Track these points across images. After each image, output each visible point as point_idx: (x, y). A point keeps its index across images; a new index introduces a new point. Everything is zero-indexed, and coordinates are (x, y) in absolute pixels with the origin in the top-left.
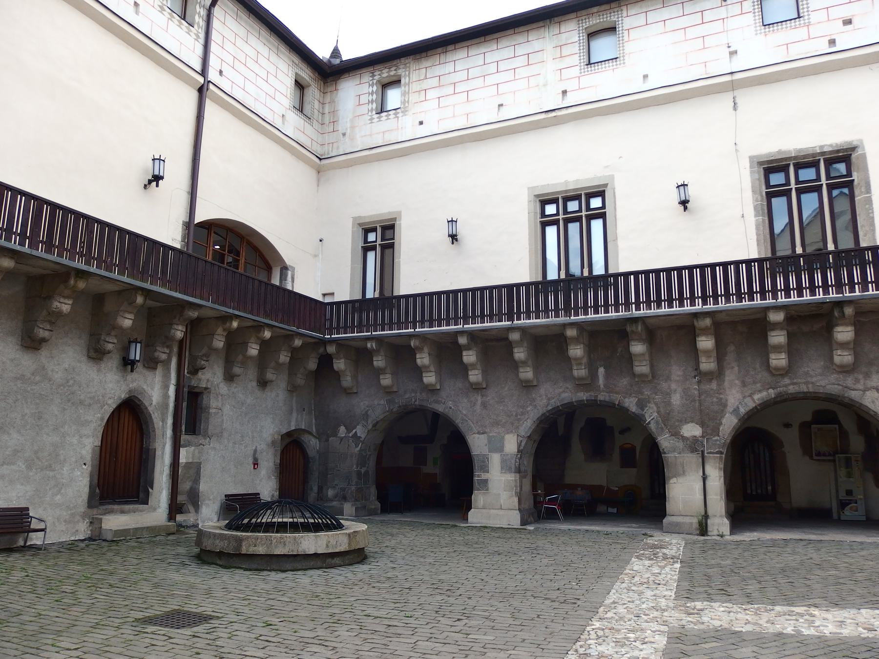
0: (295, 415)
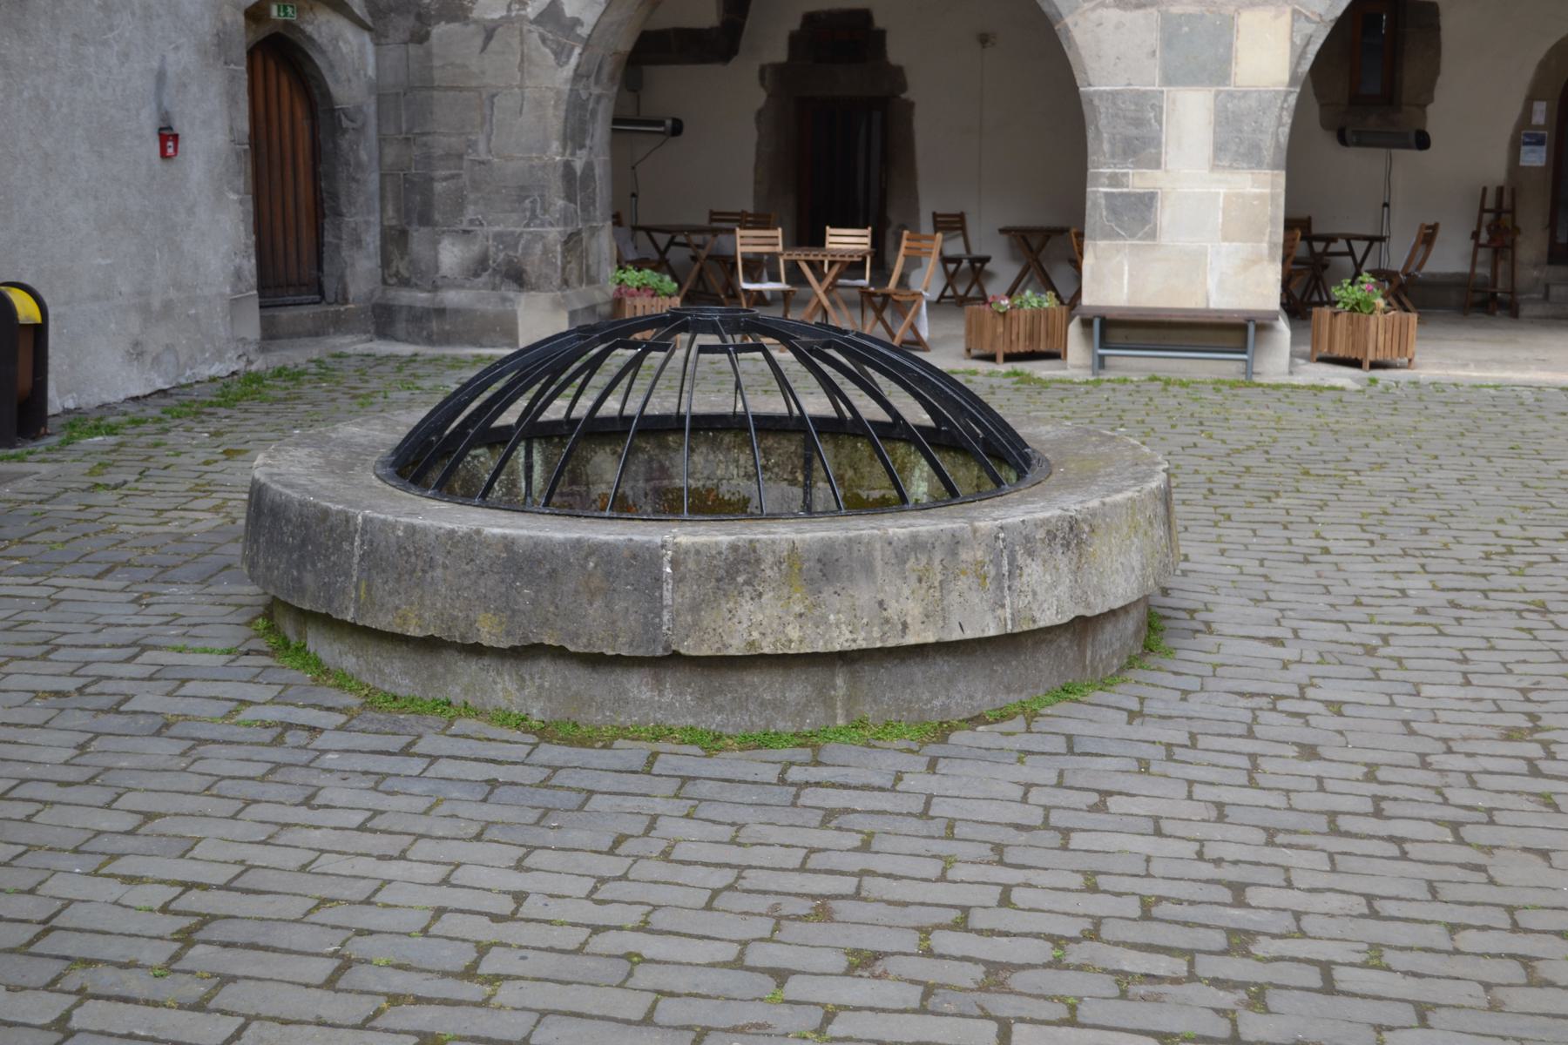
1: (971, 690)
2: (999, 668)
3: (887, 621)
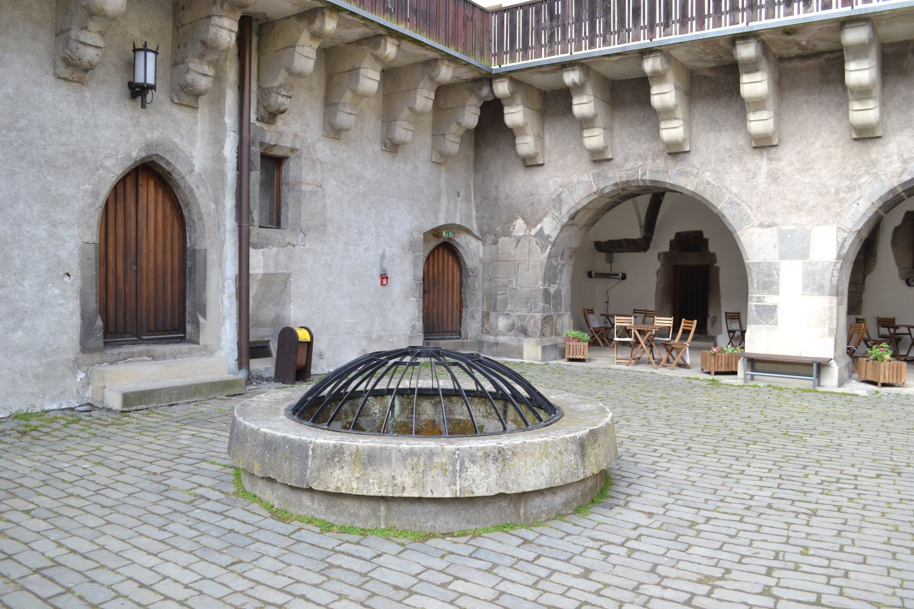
0: (444, 201)
1: (448, 520)
2: (463, 513)
3: (395, 485)
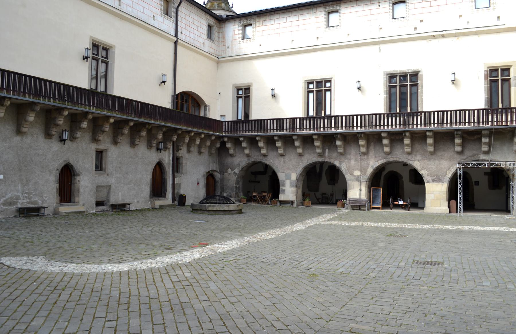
0: (211, 164)
